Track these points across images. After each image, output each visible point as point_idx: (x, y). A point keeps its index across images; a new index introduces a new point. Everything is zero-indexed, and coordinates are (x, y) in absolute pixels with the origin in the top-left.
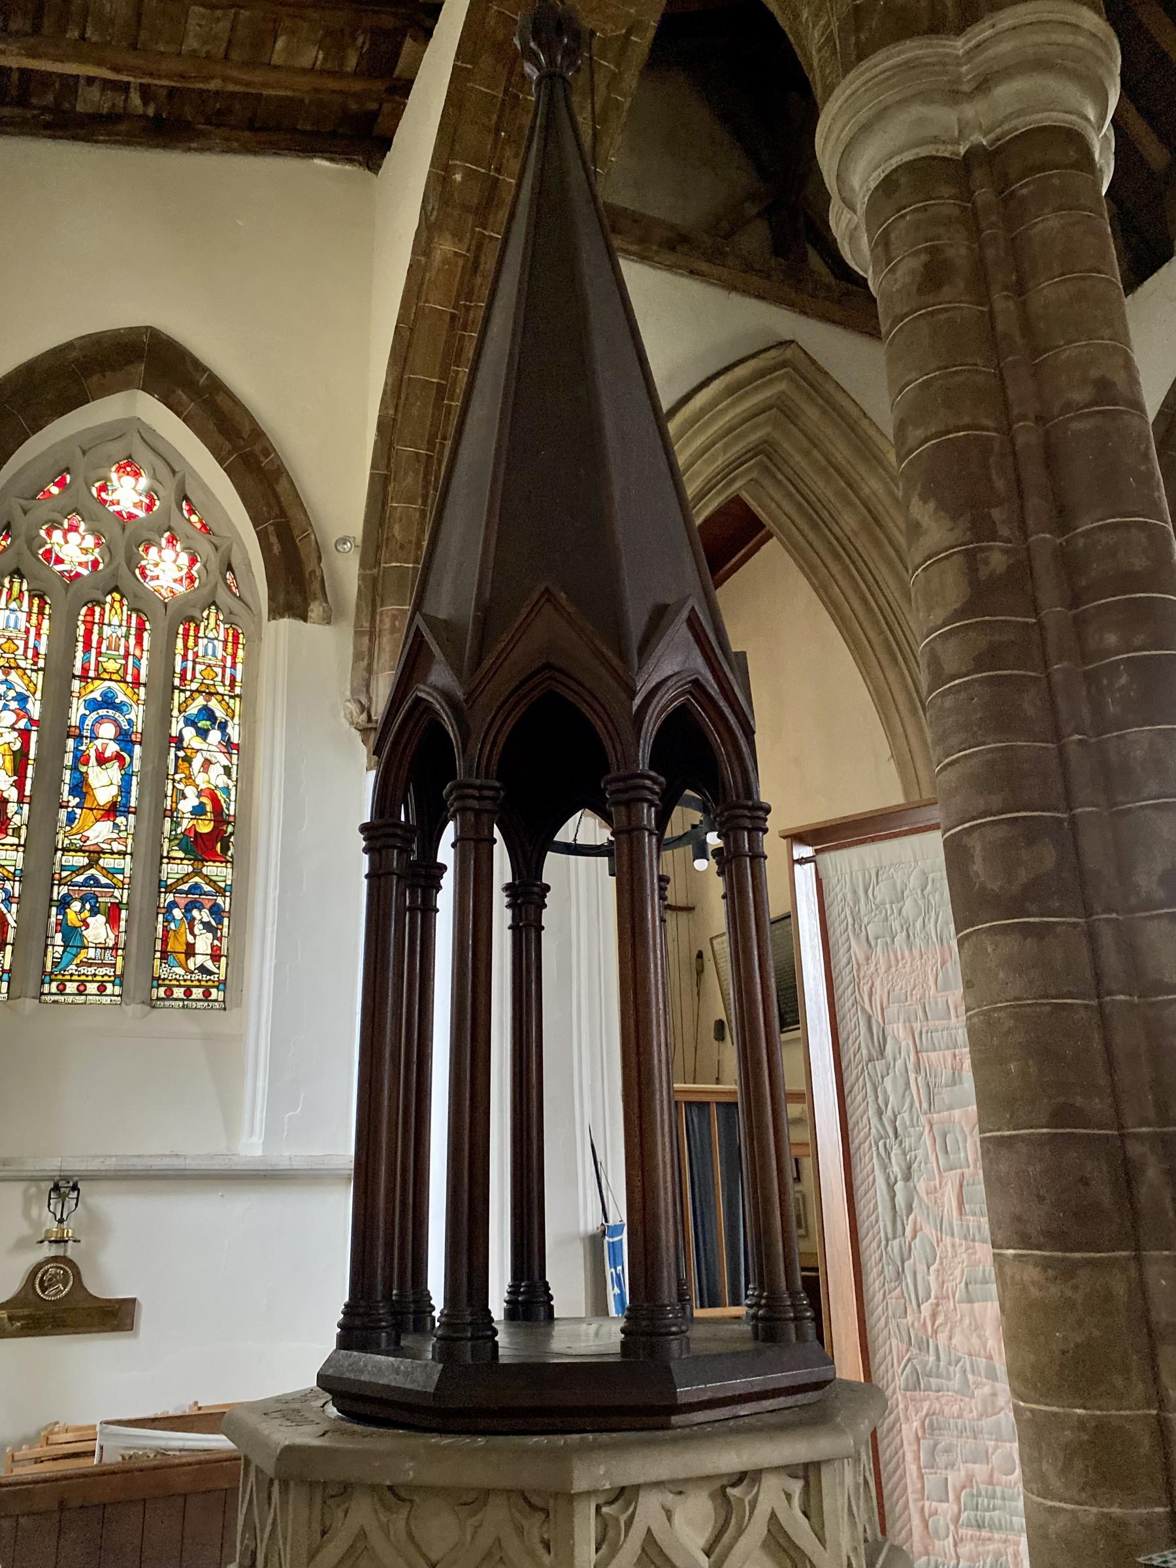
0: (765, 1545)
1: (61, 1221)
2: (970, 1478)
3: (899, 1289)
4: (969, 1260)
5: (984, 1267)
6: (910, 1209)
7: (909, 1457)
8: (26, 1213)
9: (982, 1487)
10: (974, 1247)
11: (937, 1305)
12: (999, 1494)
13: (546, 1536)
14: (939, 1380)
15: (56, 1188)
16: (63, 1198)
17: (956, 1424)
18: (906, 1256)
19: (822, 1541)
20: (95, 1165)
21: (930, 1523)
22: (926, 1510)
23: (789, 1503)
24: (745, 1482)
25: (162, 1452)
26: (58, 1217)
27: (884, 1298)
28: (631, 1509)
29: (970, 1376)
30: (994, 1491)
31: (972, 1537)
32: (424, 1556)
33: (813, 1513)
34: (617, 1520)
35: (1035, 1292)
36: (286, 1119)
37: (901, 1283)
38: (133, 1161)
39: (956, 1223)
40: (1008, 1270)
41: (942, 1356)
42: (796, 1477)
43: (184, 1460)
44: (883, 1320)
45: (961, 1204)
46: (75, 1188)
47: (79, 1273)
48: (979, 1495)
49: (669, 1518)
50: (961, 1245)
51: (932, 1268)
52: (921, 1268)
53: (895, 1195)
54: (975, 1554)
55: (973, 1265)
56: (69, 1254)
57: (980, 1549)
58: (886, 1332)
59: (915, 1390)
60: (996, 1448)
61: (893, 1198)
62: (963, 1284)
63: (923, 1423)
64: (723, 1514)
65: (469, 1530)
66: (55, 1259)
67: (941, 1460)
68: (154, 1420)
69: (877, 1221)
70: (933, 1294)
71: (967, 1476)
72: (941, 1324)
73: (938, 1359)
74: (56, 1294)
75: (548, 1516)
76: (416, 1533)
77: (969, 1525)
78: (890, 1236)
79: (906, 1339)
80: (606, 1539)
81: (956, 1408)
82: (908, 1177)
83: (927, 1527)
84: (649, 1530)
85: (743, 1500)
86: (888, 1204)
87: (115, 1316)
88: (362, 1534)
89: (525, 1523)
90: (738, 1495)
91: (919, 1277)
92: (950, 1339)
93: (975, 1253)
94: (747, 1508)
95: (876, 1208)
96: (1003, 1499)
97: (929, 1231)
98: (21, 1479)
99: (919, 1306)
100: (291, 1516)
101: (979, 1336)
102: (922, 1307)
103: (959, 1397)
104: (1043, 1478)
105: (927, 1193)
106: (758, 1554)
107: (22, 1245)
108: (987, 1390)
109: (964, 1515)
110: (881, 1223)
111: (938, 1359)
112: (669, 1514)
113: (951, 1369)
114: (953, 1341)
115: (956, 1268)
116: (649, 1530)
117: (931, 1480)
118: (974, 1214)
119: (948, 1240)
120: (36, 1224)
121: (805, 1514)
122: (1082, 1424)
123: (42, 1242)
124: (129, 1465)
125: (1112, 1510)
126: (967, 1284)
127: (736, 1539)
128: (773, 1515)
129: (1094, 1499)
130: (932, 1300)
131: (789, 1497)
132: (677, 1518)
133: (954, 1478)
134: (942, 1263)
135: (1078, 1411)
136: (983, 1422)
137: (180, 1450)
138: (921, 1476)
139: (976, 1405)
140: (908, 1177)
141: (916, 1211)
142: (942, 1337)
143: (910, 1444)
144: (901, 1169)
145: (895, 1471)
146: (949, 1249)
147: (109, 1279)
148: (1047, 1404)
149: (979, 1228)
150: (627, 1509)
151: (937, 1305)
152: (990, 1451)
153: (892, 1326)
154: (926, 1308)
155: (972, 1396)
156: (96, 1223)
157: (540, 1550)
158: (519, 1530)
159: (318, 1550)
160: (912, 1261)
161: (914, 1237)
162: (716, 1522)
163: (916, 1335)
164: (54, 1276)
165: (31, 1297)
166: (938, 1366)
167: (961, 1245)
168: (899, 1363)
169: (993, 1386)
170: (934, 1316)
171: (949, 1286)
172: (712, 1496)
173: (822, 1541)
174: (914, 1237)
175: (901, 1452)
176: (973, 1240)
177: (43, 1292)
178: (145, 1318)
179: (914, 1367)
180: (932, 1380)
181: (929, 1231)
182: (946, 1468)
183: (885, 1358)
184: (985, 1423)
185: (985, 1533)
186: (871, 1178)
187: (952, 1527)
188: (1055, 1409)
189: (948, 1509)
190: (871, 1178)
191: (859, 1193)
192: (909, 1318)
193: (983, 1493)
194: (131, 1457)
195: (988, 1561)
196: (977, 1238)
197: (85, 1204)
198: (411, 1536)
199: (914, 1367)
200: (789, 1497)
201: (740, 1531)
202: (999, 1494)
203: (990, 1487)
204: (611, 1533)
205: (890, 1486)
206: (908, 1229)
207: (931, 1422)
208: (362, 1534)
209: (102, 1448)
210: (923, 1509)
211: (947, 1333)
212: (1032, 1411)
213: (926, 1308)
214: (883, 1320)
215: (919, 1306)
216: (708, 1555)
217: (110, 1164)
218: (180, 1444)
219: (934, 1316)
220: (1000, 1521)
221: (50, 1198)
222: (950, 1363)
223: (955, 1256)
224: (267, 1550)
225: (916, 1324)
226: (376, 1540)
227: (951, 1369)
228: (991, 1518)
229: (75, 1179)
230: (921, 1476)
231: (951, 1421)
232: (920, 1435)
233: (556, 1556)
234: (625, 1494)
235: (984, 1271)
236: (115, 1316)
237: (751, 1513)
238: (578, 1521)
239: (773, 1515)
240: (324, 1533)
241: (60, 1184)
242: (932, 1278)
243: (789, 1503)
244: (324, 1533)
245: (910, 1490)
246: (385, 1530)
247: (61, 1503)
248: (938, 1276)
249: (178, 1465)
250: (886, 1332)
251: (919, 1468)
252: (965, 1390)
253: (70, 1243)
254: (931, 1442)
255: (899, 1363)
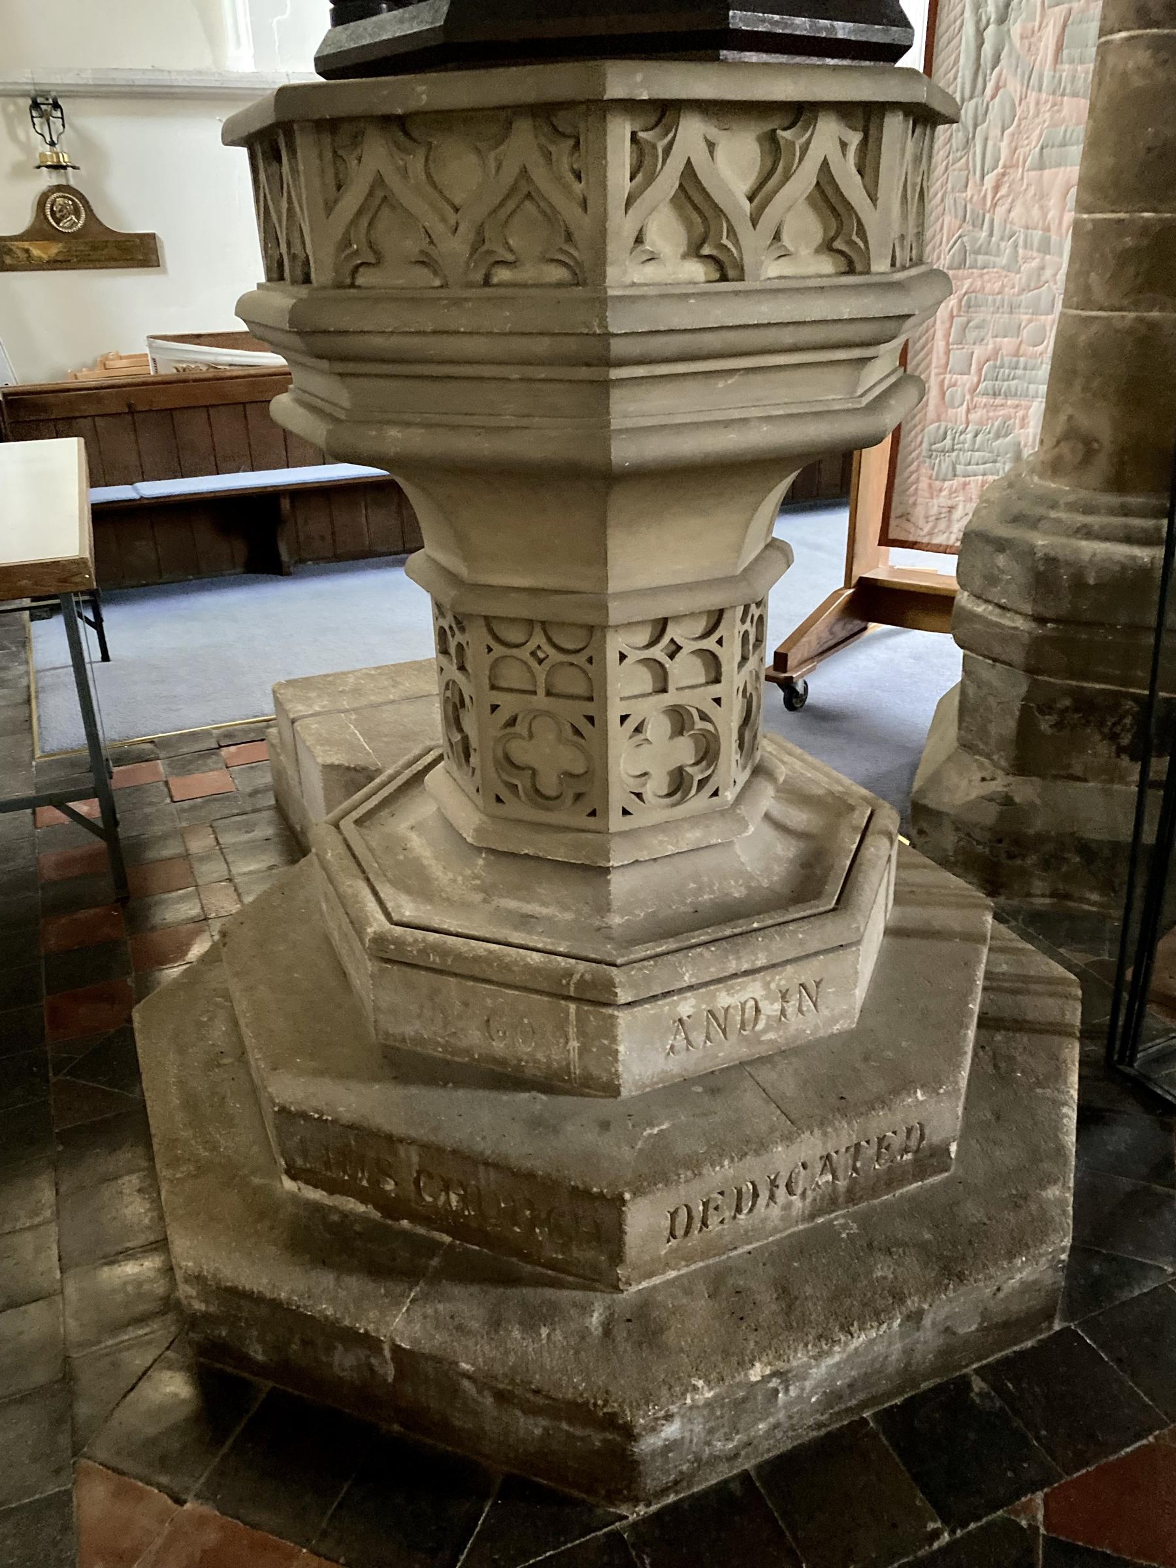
0: (810, 199)
1: (52, 144)
2: (996, 351)
3: (963, 160)
4: (1052, 118)
5: (1067, 127)
6: (997, 60)
7: (939, 334)
8: (13, 137)
9: (1007, 359)
10: (1062, 104)
11: (1003, 175)
12: (1021, 365)
13: (575, 166)
14: (987, 257)
15: (35, 105)
16: (45, 116)
17: (995, 300)
18: (980, 118)
19: (873, 199)
20: (69, 79)
21: (948, 393)
22: (946, 383)
23: (844, 155)
24: (799, 124)
25: (212, 366)
26: (48, 140)
27: (946, 169)
28: (671, 135)
29: (1021, 251)
30: (1018, 362)
31: (985, 405)
32: (448, 201)
33: (868, 171)
34: (654, 147)
35: (1138, 82)
36: (274, 24)
37: (968, 152)
38: (114, 75)
39: (1047, 73)
40: (1111, 60)
41: (995, 232)
42: (855, 130)
43: (235, 374)
44: (939, 195)
45: (1059, 48)
46: (56, 106)
47: (87, 202)
48: (1002, 367)
49: (711, 153)
50: (1046, 101)
51: (1006, 133)
52: (995, 132)
53: (983, 43)
54: (985, 417)
55: (1054, 125)
56: (72, 183)
57: (991, 414)
58: (940, 209)
59: (959, 268)
60: (1030, 321)
61: (980, 44)
62: (1037, 149)
63: (960, 301)
64: (769, 164)
65: (493, 165)
66: (58, 188)
67: (971, 335)
68: (199, 336)
69: (955, 78)
70: (1001, 163)
71: (994, 348)
72: (1003, 197)
73: (991, 234)
74: (70, 227)
75: (578, 143)
76: (436, 178)
77: (986, 394)
78: (967, 94)
79: (960, 213)
80: (644, 164)
81: (997, 286)
82: (1002, 19)
83: (943, 394)
84: (689, 162)
85: (794, 143)
86: (973, 55)
87: (139, 252)
88: (379, 181)
89: (552, 148)
90: (789, 138)
91: (990, 143)
92: (1009, 211)
93: (1059, 111)
94: (798, 154)
95: (957, 61)
96: (1025, 369)
97: (1014, 87)
98: (86, 385)
99: (983, 177)
100: (303, 184)
101: (1041, 207)
102: (986, 178)
103: (1004, 273)
104: (1087, 289)
105: (1022, 38)
106: (803, 208)
107: (18, 172)
108: (1035, 264)
109: (982, 386)
110: (959, 80)
111: (991, 234)
112: (711, 146)
113: (1003, 244)
114: (1012, 214)
115: (1034, 129)
116: (689, 162)
117: (957, 355)
118: (1072, 61)
119: (1032, 96)
120: (26, 147)
121: (859, 172)
122: (1146, 226)
123: (39, 167)
124: (184, 376)
125: (1152, 314)
126: (1042, 148)
127: (783, 183)
128: (825, 164)
129: (1136, 305)
130: (999, 170)
131: (844, 145)
132: (719, 152)
133: (979, 352)
134: (1019, 125)
135: (1146, 215)
136: (1023, 297)
137: (231, 365)
138: (948, 352)
139: (1019, 279)
140: (1002, 19)
141: (1003, 62)
142: (1000, 210)
143: (943, 322)
144: (997, 7)
145: (922, 349)
146: (1032, 106)
147: (126, 214)
148: (1113, 211)
149: (1074, 77)
150: (667, 135)
151: (1003, 175)
152: (1023, 324)
153: (949, 201)
154: (990, 180)
155: (1018, 272)
156: (88, 144)
157: (570, 177)
158: (548, 156)
159: (336, 202)
160: (985, 125)
161: (993, 98)
162: (762, 165)
163: (973, 211)
164: (64, 206)
165: (45, 226)
166: (990, 242)
167: (1046, 101)
168: (948, 241)
169: (1043, 259)
170: (997, 188)
171: (1021, 152)
172: (760, 139)
173: (873, 199)
174: (993, 98)
175: (931, 331)
176: (1063, 95)
177: (58, 224)
178: (168, 251)
179: (963, 243)
180: (980, 257)
181: (1014, 87)
182: (974, 344)
183: (934, 236)
184: (1027, 297)
185: (998, 401)
186: (958, 23)
187: (968, 397)
188: (1122, 215)
189: (969, 380)
190: (958, 23)
191: (941, 42)
192: (969, 192)
193: (1007, 365)
194: (184, 370)
195: (996, 424)
196: (1068, 91)
197: (72, 126)
198: (429, 176)
199: (963, 243)
200: (844, 145)
201: (787, 177)
202: (1021, 365)
203: (1015, 359)
204: (647, 161)
205: (914, 363)
206: (990, 86)
207: (969, 300)
208: (379, 181)
209: (154, 360)
210: (943, 381)
211: (1007, 206)
212: (1093, 220)
213: (990, 180)
214: (939, 195)
215: (983, 177)
216: (751, 199)
217: (87, 78)
218: (228, 359)
219: (997, 188)
220: (1016, 389)
221: (32, 117)
222: (1002, 239)
223: (1037, 114)
224: (287, 234)
225: (975, 198)
226: (393, 180)
227: (1003, 244)
228: (1009, 387)
229: (53, 94)
230: (948, 352)
231: (990, 298)
232: (955, 313)
233: (587, 183)
234: (665, 112)
235: (1066, 131)
236: (139, 252)
237: (801, 160)
238: (610, 141)
239: (825, 164)
240: (339, 188)
241: (39, 100)
242: (1004, 145)
243: (844, 155)
244: (339, 188)
245: (933, 365)
246: (404, 172)
247: (130, 406)
248: (1011, 142)
249: (232, 378)
250: (940, 209)
251: (948, 344)
252: (1013, 266)
253: (70, 169)
254: (964, 319)
255: (948, 241)
